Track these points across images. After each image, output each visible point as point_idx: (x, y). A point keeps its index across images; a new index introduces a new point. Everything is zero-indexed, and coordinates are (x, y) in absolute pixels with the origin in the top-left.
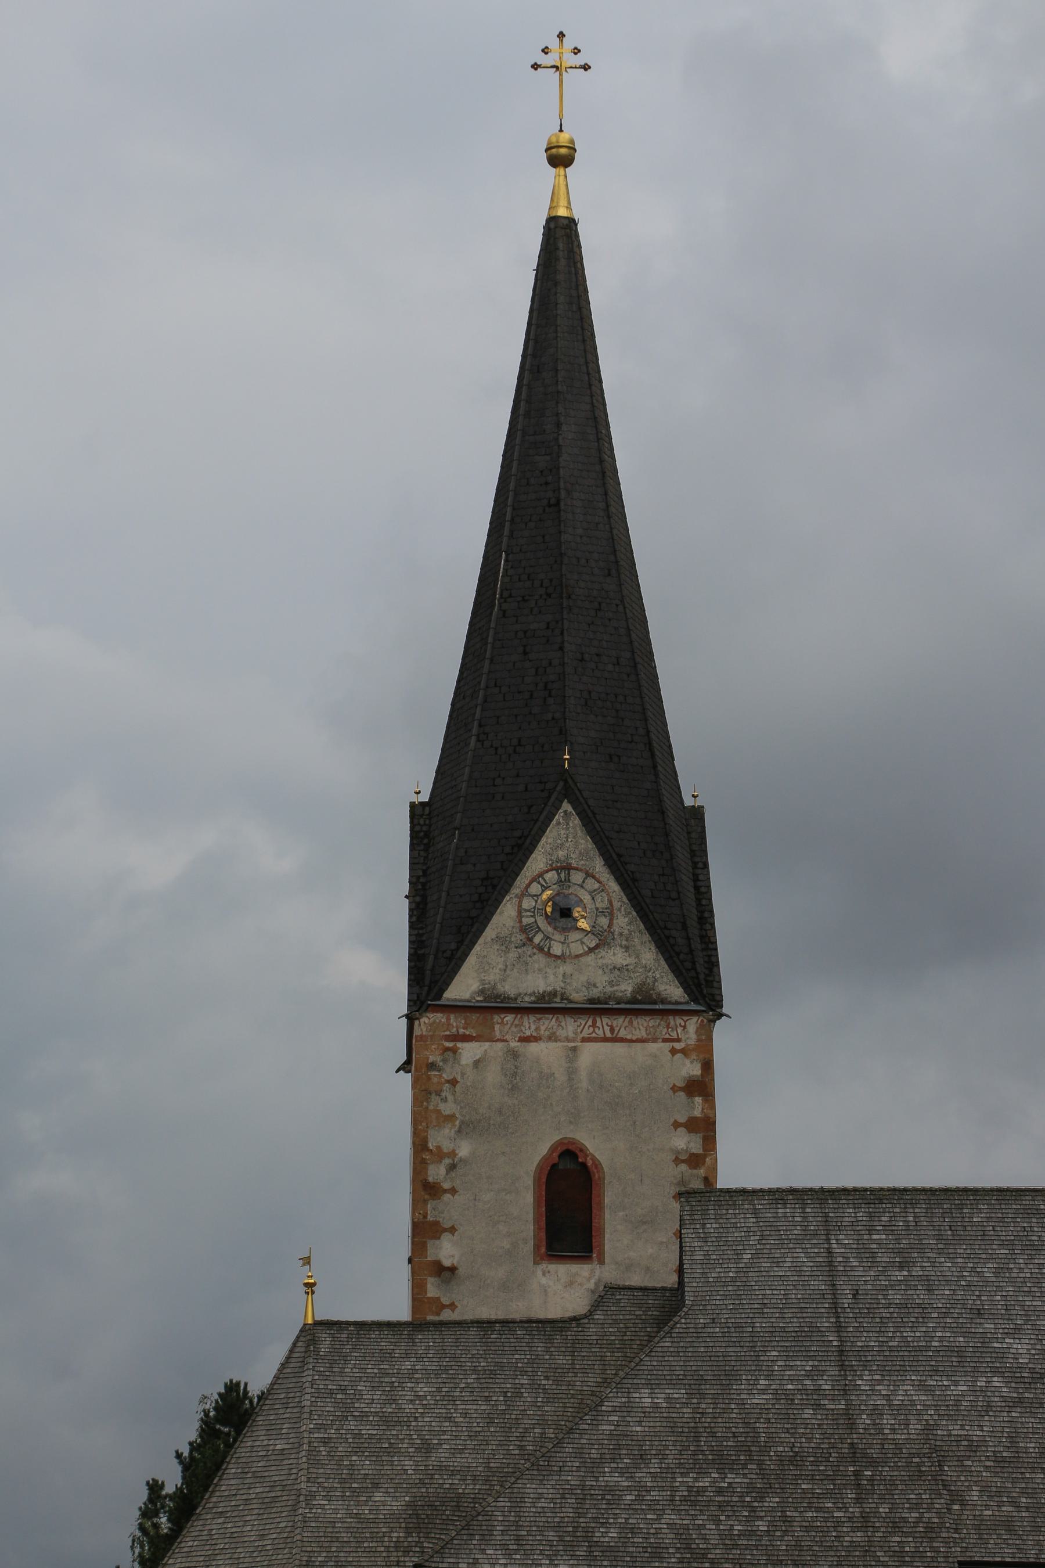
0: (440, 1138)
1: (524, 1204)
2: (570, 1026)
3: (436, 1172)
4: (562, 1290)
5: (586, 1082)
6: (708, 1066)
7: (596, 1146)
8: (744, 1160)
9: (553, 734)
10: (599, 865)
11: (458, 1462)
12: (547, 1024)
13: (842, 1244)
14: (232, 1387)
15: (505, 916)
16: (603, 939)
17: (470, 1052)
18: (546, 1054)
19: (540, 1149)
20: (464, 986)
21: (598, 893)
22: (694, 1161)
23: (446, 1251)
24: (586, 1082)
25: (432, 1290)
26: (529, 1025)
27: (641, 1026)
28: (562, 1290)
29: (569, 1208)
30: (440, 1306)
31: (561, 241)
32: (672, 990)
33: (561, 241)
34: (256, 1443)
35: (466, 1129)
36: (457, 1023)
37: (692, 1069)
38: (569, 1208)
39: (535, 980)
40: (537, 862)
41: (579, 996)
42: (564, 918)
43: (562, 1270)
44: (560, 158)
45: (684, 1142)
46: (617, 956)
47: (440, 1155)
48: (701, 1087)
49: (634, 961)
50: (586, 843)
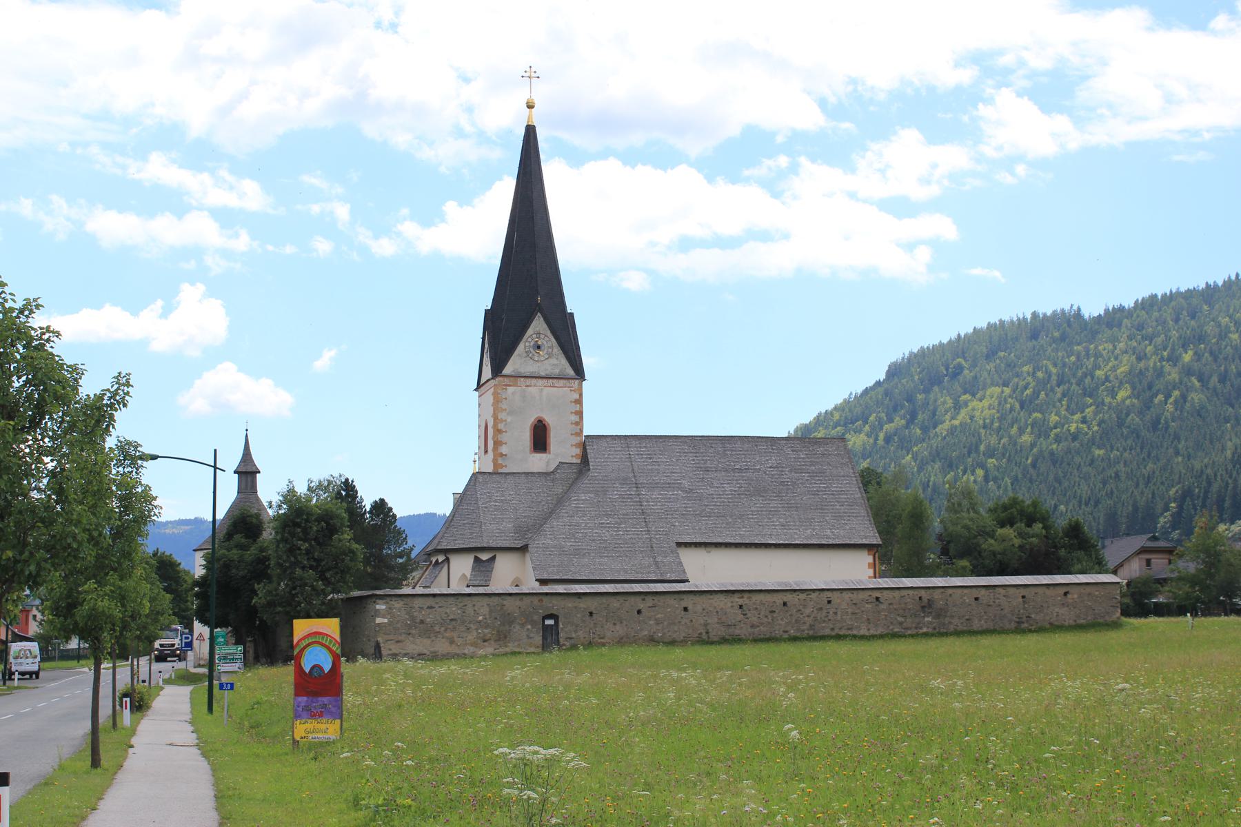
0: (501, 416)
1: (527, 437)
2: (540, 382)
3: (501, 426)
4: (538, 462)
5: (541, 400)
6: (581, 395)
7: (549, 419)
8: (591, 427)
9: (527, 298)
10: (549, 333)
11: (525, 514)
12: (534, 381)
13: (633, 451)
14: (382, 501)
15: (521, 348)
16: (550, 356)
17: (510, 389)
18: (533, 390)
19: (531, 420)
20: (508, 370)
21: (549, 341)
22: (577, 423)
23: (504, 449)
24: (541, 400)
25: (500, 461)
26: (528, 381)
27: (562, 382)
28: (538, 462)
29: (540, 438)
30: (502, 466)
31: (530, 132)
32: (571, 372)
33: (530, 132)
34: (545, 576)
35: (510, 413)
36: (506, 380)
37: (577, 396)
38: (540, 438)
39: (530, 368)
40: (530, 331)
41: (543, 374)
42: (535, 352)
43: (538, 456)
44: (530, 106)
45: (574, 418)
46: (553, 361)
47: (502, 421)
48: (579, 401)
49: (559, 363)
50: (545, 326)
